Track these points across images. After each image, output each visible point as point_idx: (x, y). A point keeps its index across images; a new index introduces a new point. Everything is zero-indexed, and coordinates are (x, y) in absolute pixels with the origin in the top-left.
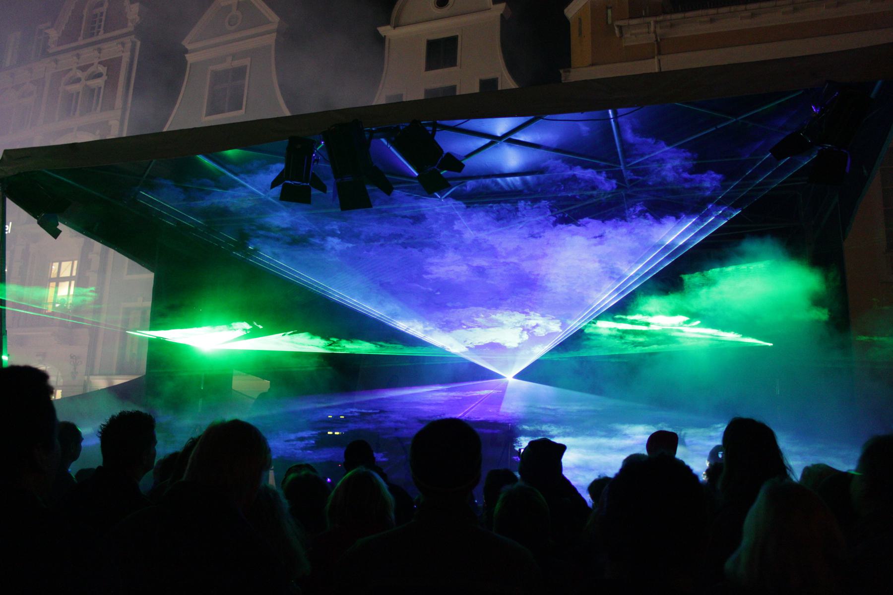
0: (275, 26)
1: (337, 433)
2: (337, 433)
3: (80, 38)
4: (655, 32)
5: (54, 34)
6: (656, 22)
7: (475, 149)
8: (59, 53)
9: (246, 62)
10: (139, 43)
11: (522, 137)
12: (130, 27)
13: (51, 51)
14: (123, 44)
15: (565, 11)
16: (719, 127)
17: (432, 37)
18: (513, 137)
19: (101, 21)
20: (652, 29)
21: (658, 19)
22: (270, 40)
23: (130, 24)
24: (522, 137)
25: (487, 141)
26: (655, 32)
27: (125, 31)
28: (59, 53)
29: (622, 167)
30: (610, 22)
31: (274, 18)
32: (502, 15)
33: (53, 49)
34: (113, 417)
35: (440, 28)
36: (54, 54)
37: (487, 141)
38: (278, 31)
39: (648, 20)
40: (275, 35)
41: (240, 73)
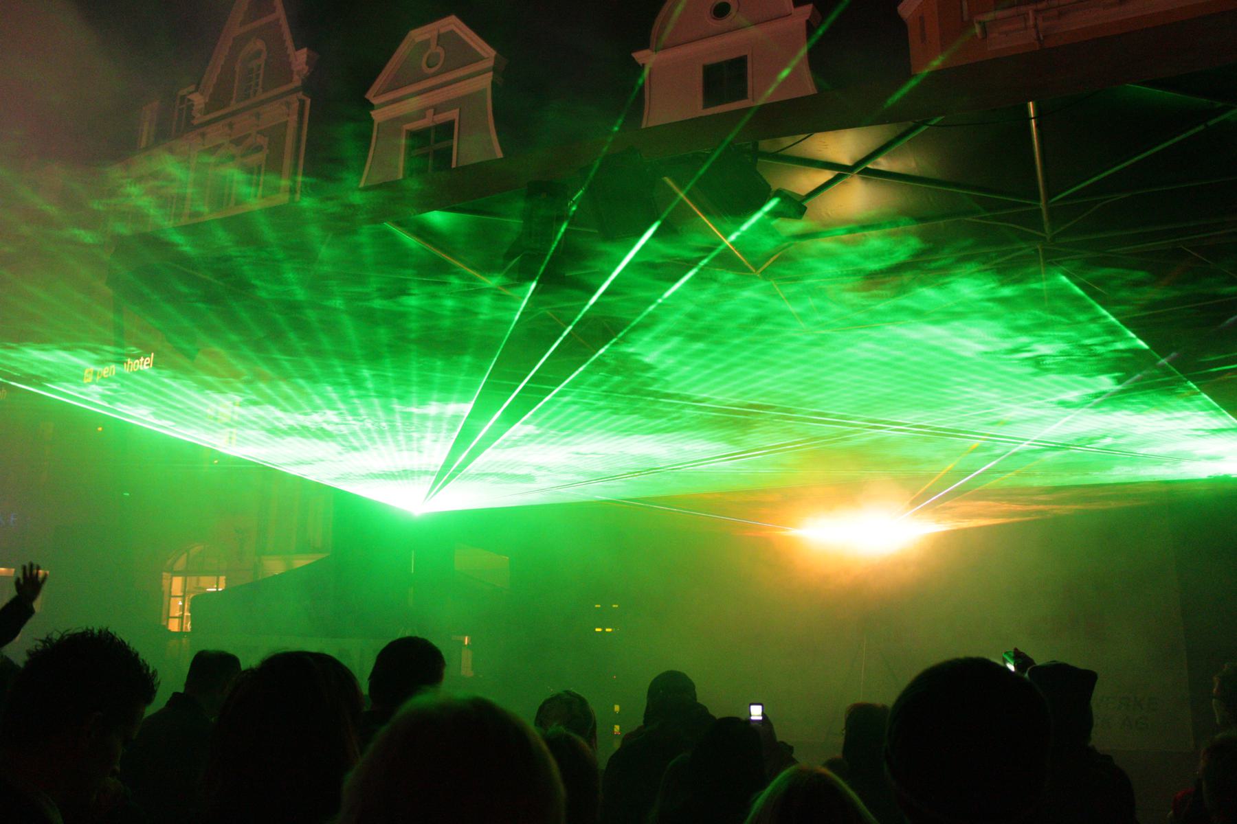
0: (489, 64)
1: (608, 630)
2: (608, 630)
3: (233, 102)
4: (1036, 26)
5: (198, 100)
6: (1037, 11)
7: (811, 189)
8: (209, 123)
9: (453, 115)
10: (308, 102)
11: (882, 163)
12: (297, 82)
13: (195, 122)
14: (288, 104)
15: (899, 8)
16: (1201, 127)
17: (708, 61)
18: (870, 166)
19: (258, 76)
20: (1031, 23)
21: (1040, 6)
22: (484, 83)
23: (296, 77)
24: (882, 163)
25: (828, 175)
26: (1036, 26)
27: (292, 86)
28: (209, 123)
29: (1042, 204)
30: (966, 18)
31: (488, 53)
32: (808, 21)
33: (199, 118)
34: (48, 640)
35: (718, 48)
36: (202, 125)
37: (828, 175)
38: (495, 69)
39: (1023, 9)
40: (491, 74)
41: (446, 129)
